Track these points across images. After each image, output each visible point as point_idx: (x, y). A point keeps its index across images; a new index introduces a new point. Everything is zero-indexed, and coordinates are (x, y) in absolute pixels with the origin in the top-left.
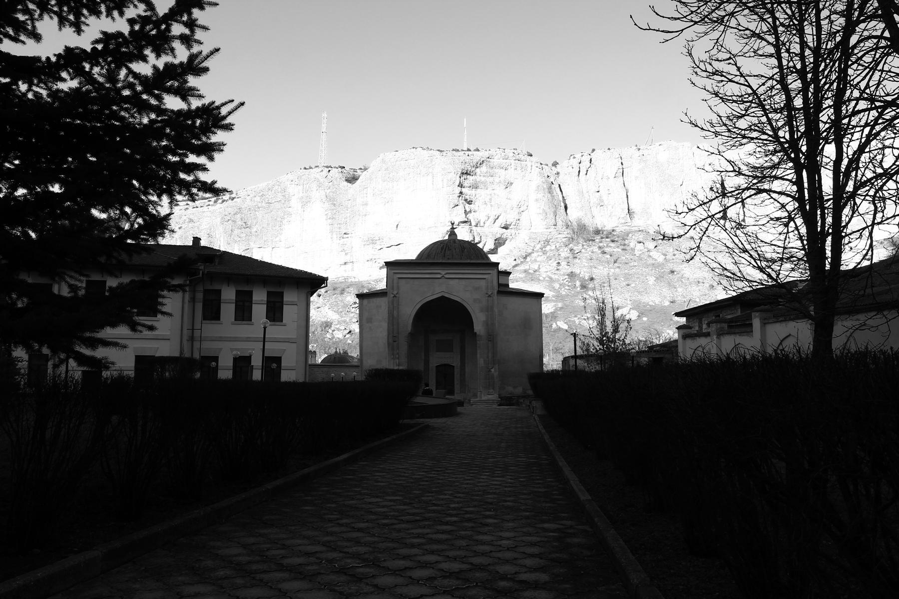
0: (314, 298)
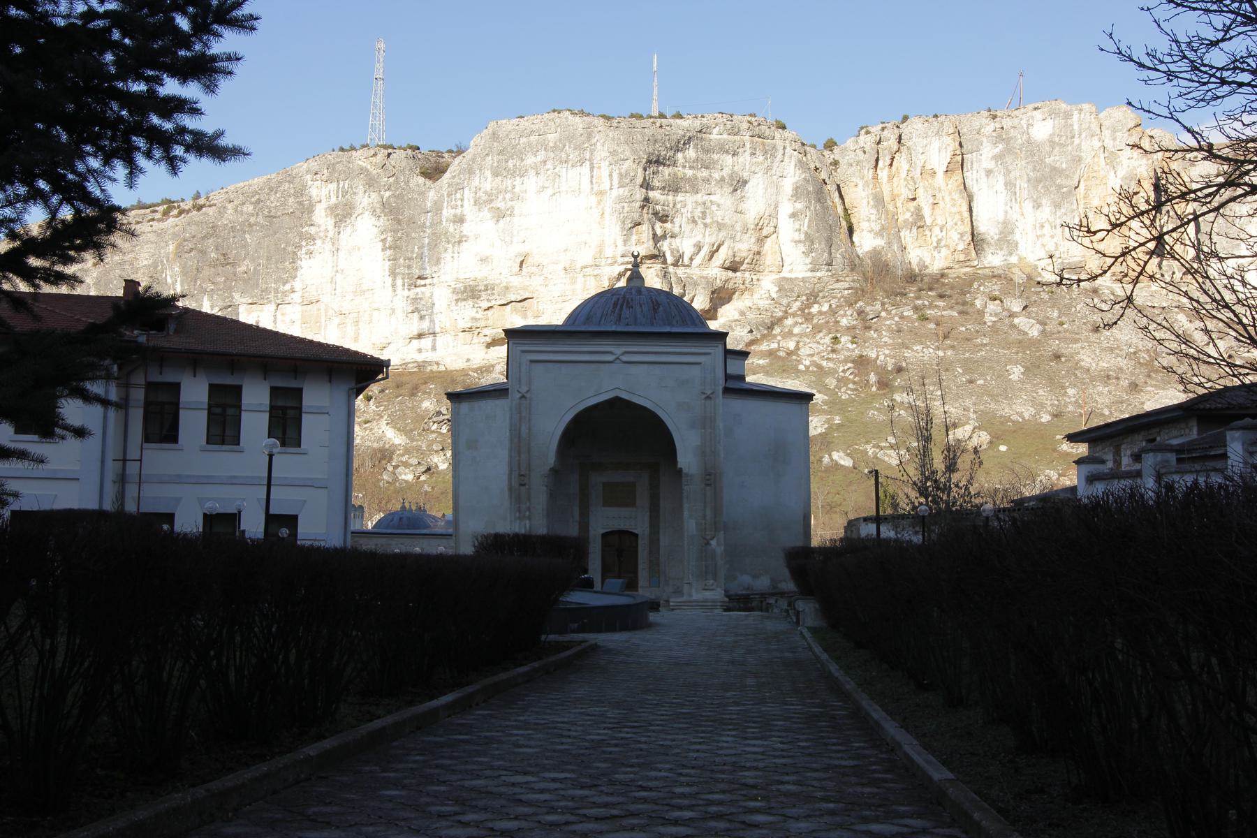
0: (360, 401)
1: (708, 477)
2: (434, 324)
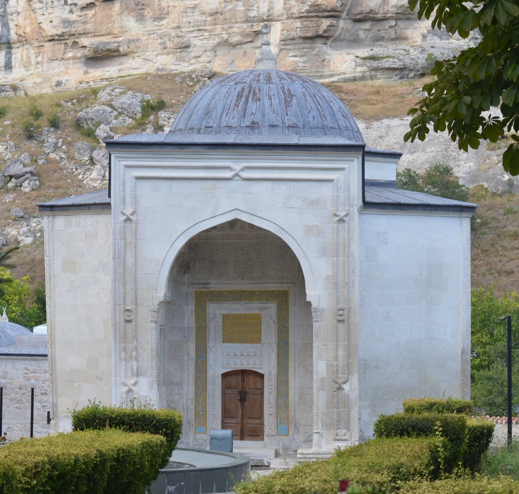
1: (341, 312)
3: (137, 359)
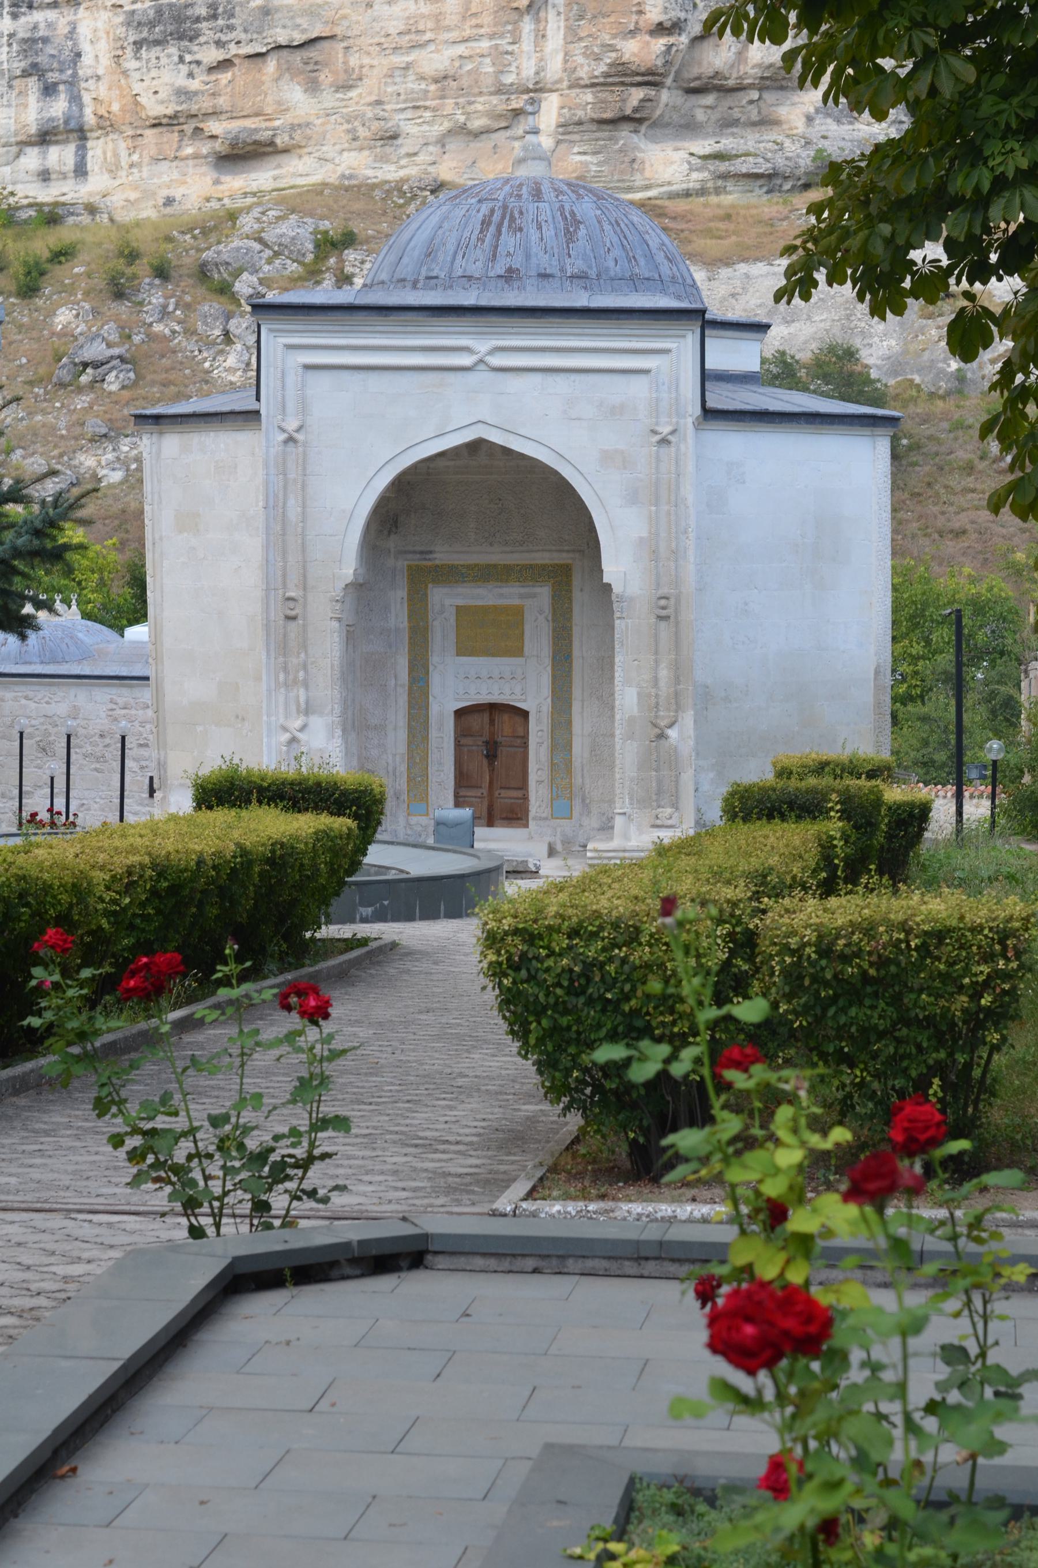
1: (663, 602)
2: (81, 106)
3: (306, 685)
